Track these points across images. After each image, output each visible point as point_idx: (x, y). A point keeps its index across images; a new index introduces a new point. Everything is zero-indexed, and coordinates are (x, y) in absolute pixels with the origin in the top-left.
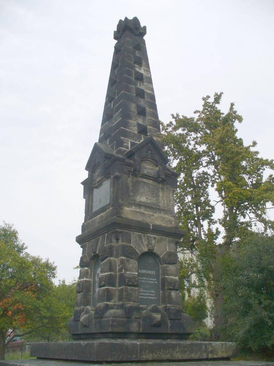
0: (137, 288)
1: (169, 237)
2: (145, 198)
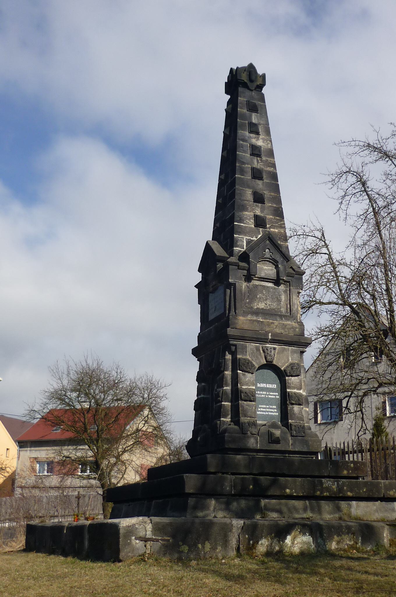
0: (254, 403)
1: (292, 347)
2: (263, 304)
